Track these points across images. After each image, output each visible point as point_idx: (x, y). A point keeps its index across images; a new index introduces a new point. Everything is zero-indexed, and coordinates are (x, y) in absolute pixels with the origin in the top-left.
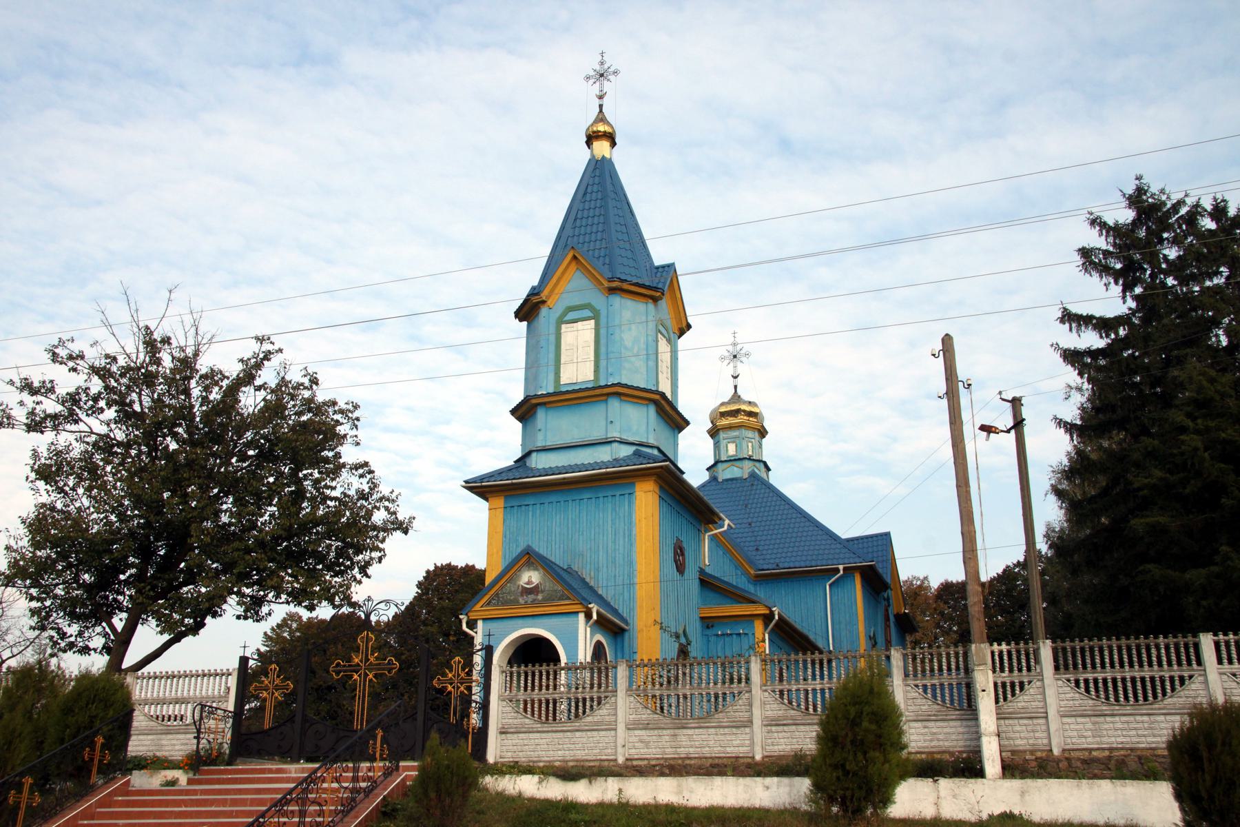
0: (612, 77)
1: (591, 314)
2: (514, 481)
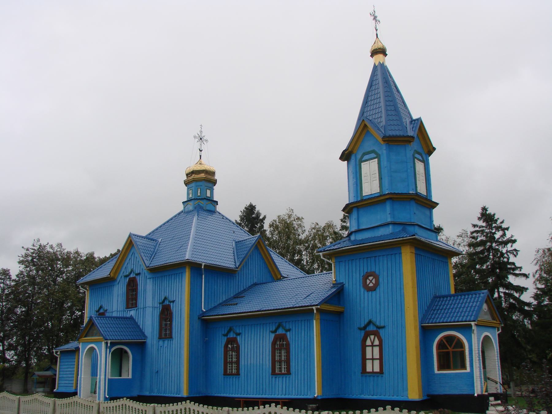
1: (375, 156)
2: (360, 245)
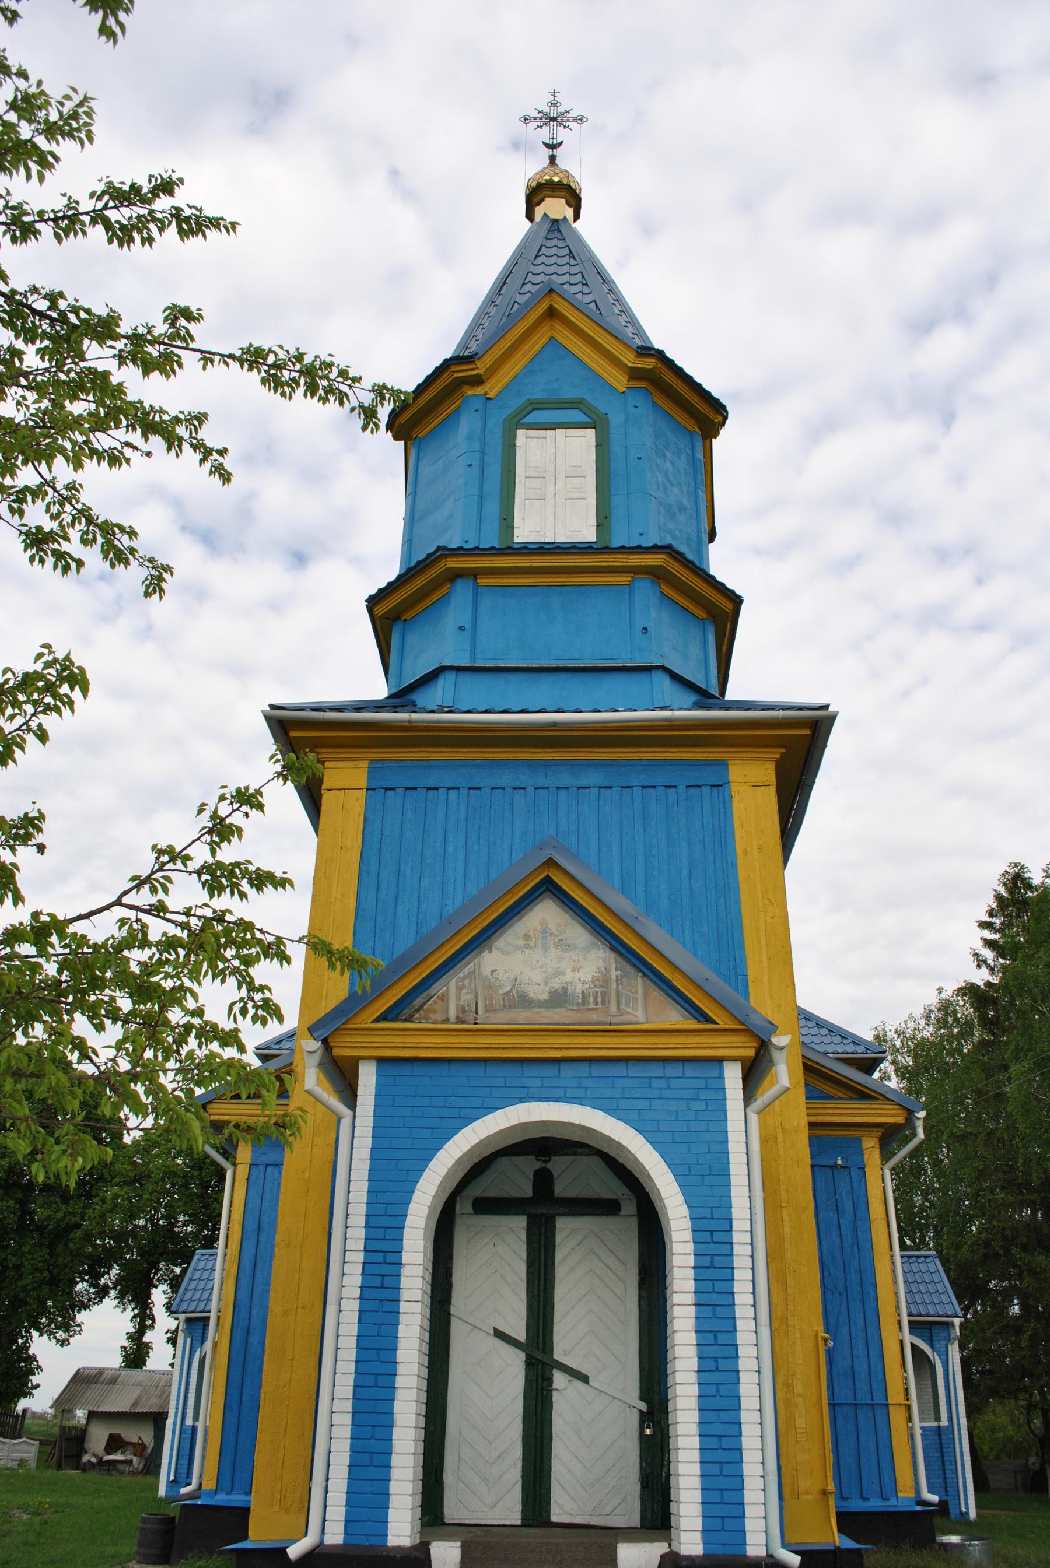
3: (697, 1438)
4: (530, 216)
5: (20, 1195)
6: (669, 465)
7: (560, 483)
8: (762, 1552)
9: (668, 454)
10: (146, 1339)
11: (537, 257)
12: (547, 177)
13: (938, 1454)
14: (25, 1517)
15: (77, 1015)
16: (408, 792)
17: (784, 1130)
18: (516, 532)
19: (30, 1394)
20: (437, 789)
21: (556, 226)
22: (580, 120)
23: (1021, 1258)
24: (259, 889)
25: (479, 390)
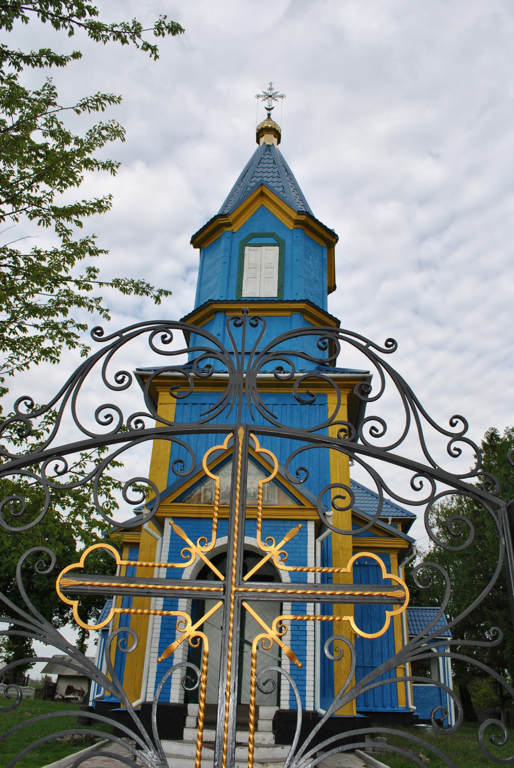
0: (279, 99)
1: (275, 242)
3: (289, 666)
4: (258, 142)
5: (28, 575)
6: (311, 262)
7: (263, 271)
8: (312, 709)
9: (311, 257)
10: (85, 643)
11: (259, 163)
12: (266, 125)
13: (439, 699)
14: (30, 714)
15: (57, 505)
16: (194, 406)
17: (342, 549)
18: (243, 292)
19: (31, 667)
20: (205, 404)
21: (269, 148)
22: (282, 96)
23: (487, 612)
24: (113, 466)
25: (230, 229)
